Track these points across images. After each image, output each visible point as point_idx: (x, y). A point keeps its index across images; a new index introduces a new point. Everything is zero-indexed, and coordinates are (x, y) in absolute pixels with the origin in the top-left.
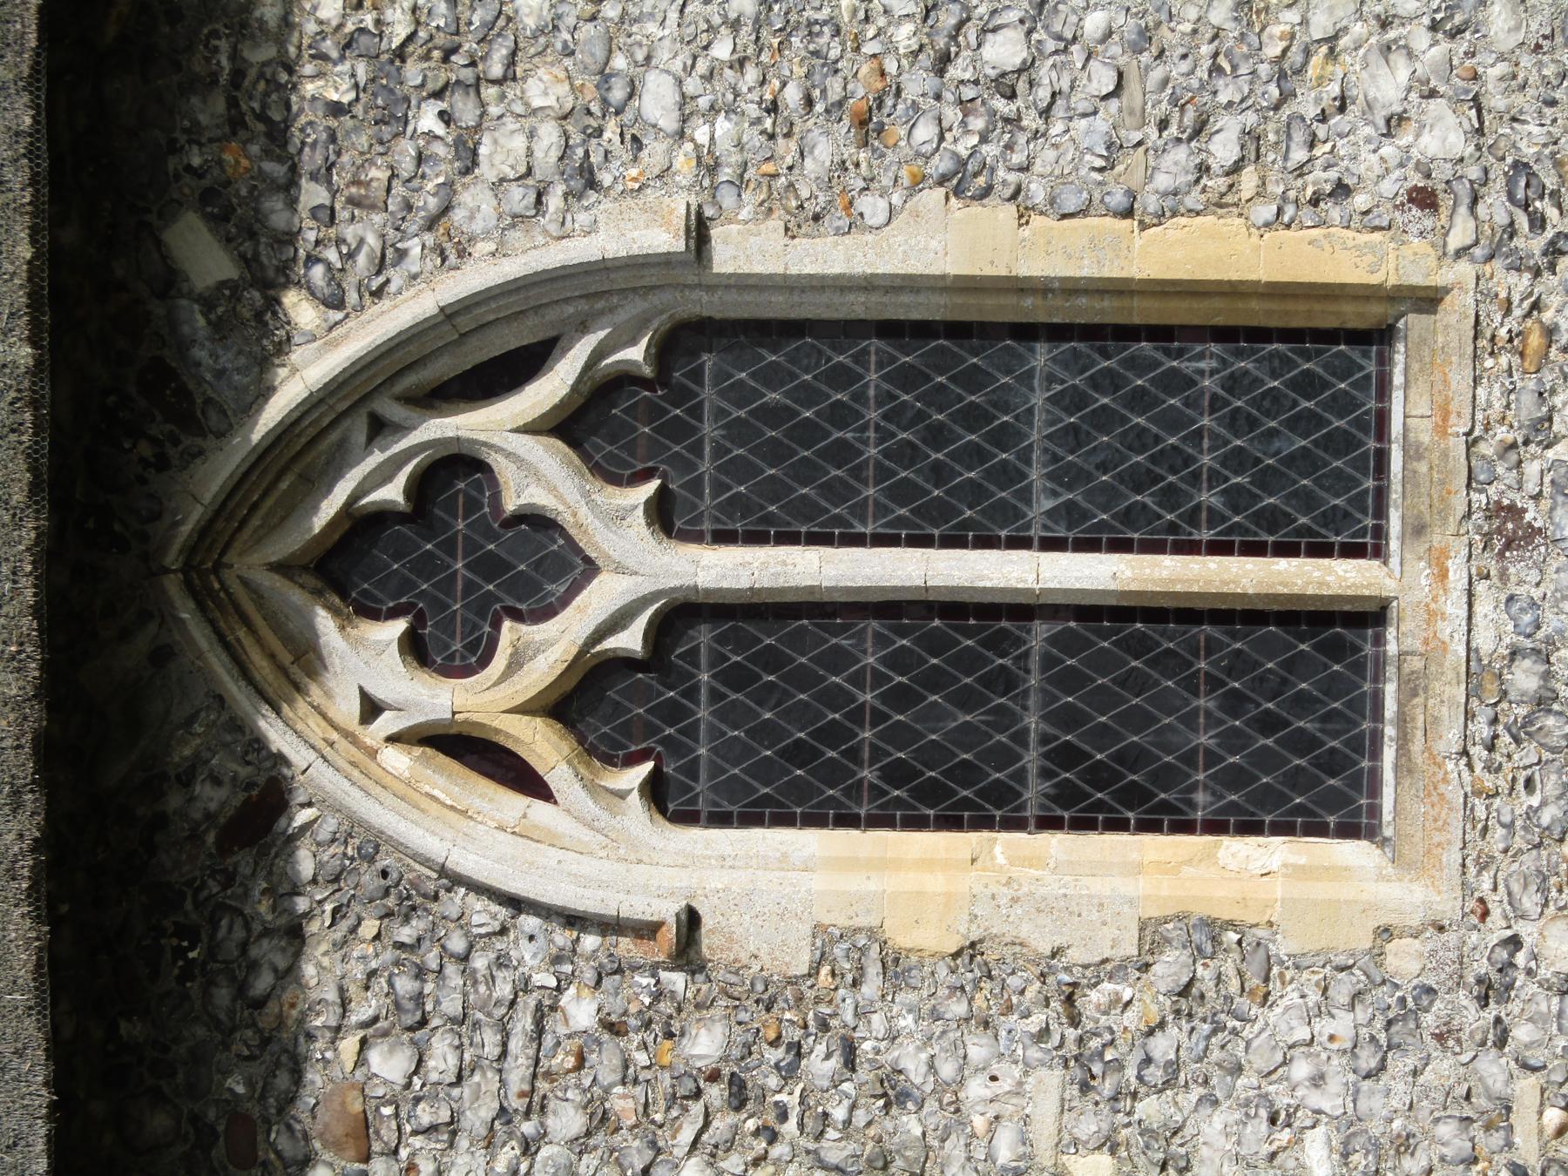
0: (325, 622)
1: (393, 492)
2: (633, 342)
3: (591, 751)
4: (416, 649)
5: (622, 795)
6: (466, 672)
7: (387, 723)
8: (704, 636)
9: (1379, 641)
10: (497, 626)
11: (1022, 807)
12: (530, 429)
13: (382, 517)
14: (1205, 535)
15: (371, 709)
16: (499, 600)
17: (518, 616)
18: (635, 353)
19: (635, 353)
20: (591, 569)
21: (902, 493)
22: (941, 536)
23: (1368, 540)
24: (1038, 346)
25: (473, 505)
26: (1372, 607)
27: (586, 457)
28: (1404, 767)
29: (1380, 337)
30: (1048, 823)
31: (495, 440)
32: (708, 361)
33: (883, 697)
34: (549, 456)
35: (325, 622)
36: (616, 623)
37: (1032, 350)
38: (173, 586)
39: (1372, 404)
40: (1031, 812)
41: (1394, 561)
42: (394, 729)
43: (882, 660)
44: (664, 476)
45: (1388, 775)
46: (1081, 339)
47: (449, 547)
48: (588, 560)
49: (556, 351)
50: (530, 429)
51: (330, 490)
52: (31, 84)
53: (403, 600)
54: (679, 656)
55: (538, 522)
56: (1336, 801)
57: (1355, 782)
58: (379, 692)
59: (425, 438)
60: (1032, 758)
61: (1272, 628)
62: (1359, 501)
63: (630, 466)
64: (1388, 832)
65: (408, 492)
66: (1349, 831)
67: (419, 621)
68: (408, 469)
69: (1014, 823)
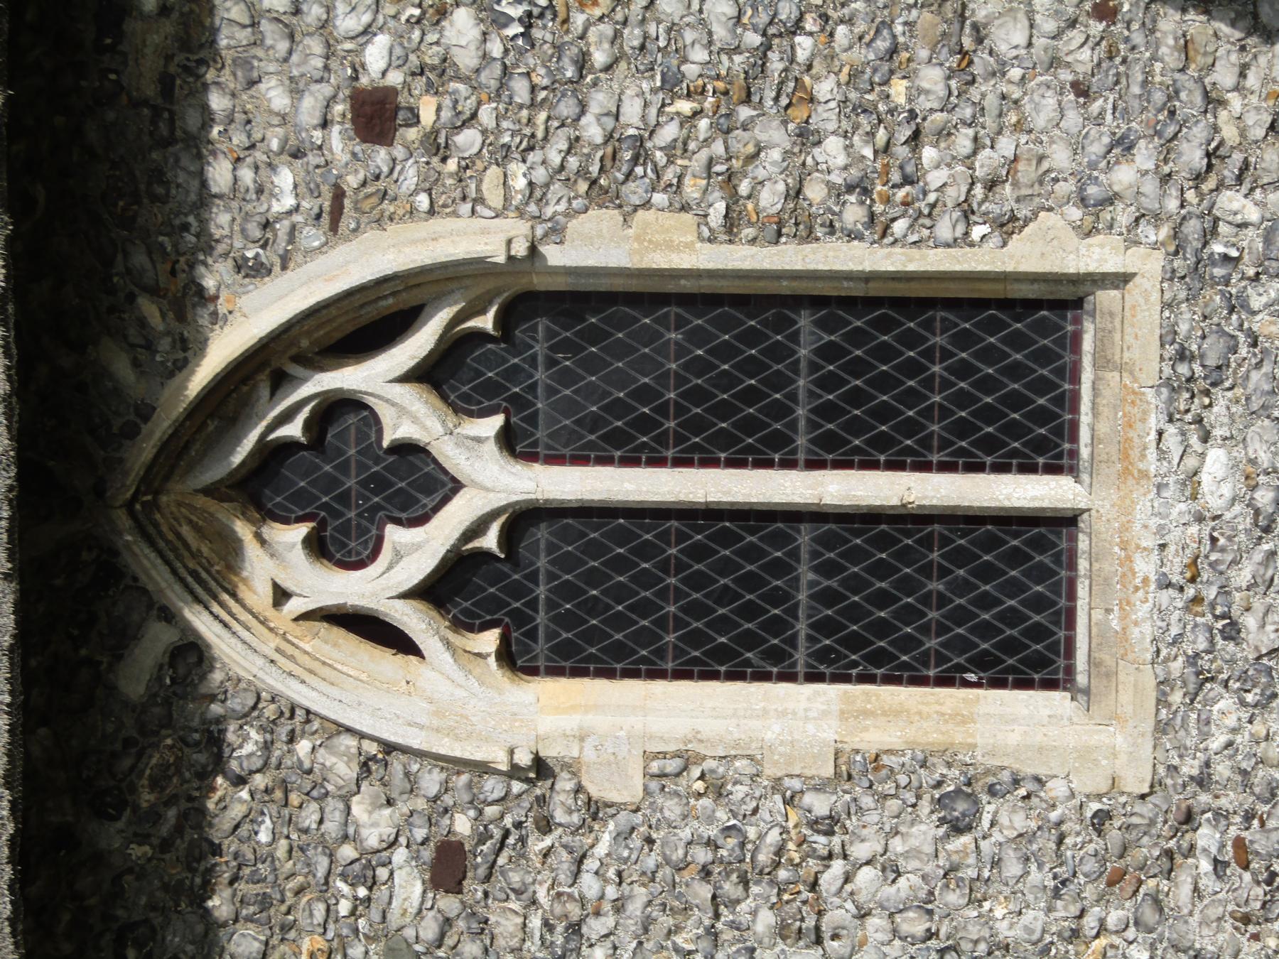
0: (243, 530)
1: (294, 430)
2: (483, 311)
3: (457, 410)
4: (318, 547)
5: (478, 440)
6: (360, 565)
7: (295, 606)
8: (542, 533)
9: (1073, 539)
10: (381, 529)
11: (794, 451)
12: (406, 378)
13: (289, 446)
14: (935, 458)
15: (281, 595)
16: (383, 508)
17: (398, 522)
18: (486, 322)
19: (486, 322)
20: (456, 486)
21: (695, 638)
22: (726, 459)
23: (1061, 676)
24: (802, 527)
25: (362, 436)
26: (1070, 514)
27: (444, 398)
28: (1102, 362)
29: (1078, 303)
30: (814, 677)
31: (378, 391)
32: (542, 324)
33: (681, 609)
34: (416, 400)
35: (243, 530)
36: (477, 529)
37: (799, 532)
38: (123, 520)
39: (1070, 328)
40: (800, 669)
41: (1085, 477)
42: (304, 609)
43: (681, 609)
44: (506, 411)
45: (1087, 362)
46: (835, 522)
47: (344, 468)
48: (454, 480)
49: (423, 315)
50: (406, 378)
51: (245, 436)
52: (11, 888)
53: (308, 510)
54: (524, 332)
55: (409, 450)
56: (1041, 446)
57: (1059, 431)
58: (287, 584)
59: (318, 389)
60: (802, 628)
61: (989, 527)
62: (1054, 648)
63: (479, 617)
64: (1081, 679)
65: (307, 426)
66: (1050, 685)
67: (322, 525)
68: (313, 404)
69: (788, 677)
